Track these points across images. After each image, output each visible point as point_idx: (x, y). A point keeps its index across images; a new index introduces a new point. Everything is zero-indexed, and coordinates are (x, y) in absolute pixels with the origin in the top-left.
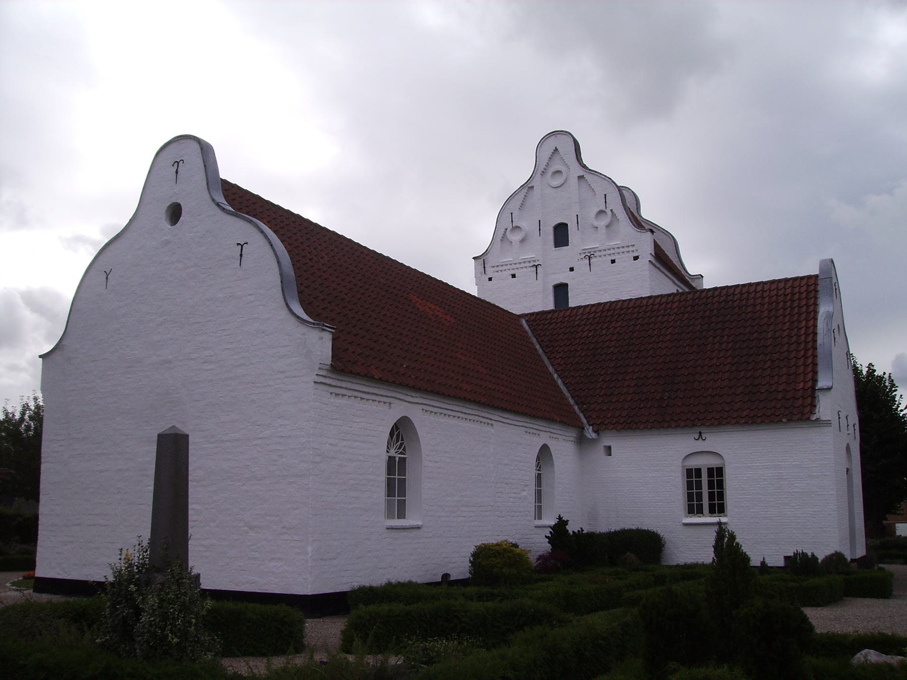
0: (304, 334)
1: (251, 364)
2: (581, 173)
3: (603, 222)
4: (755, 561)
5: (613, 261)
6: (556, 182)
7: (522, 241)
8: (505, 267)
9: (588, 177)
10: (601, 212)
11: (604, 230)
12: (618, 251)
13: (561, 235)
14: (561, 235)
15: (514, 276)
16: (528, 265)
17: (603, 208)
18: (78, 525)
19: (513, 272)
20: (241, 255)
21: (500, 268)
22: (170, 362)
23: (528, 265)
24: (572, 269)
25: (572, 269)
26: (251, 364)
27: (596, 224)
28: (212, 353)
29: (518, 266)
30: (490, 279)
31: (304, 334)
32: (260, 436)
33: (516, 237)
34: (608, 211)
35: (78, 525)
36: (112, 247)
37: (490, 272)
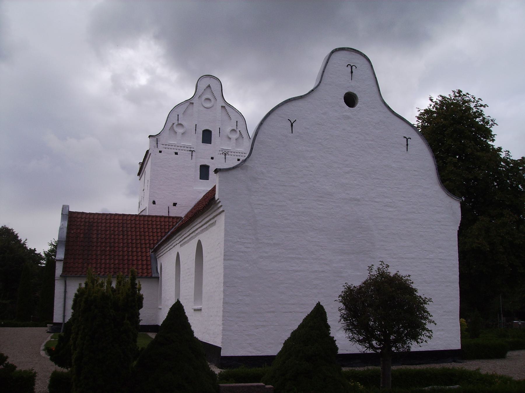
0: (450, 202)
1: (420, 213)
2: (224, 105)
3: (234, 136)
4: (331, 335)
5: (176, 153)
6: (208, 105)
7: (183, 134)
8: (170, 147)
9: (228, 108)
10: (233, 130)
11: (235, 141)
12: (242, 154)
13: (207, 136)
14: (207, 136)
15: (176, 153)
16: (186, 149)
17: (235, 128)
18: (273, 312)
19: (176, 151)
20: (407, 145)
21: (167, 146)
22: (359, 200)
23: (186, 149)
24: (212, 158)
25: (212, 158)
26: (420, 213)
27: (230, 136)
28: (391, 201)
29: (179, 148)
30: (160, 152)
31: (450, 202)
32: (428, 257)
33: (180, 130)
34: (238, 131)
35: (273, 312)
36: (284, 107)
37: (161, 148)
